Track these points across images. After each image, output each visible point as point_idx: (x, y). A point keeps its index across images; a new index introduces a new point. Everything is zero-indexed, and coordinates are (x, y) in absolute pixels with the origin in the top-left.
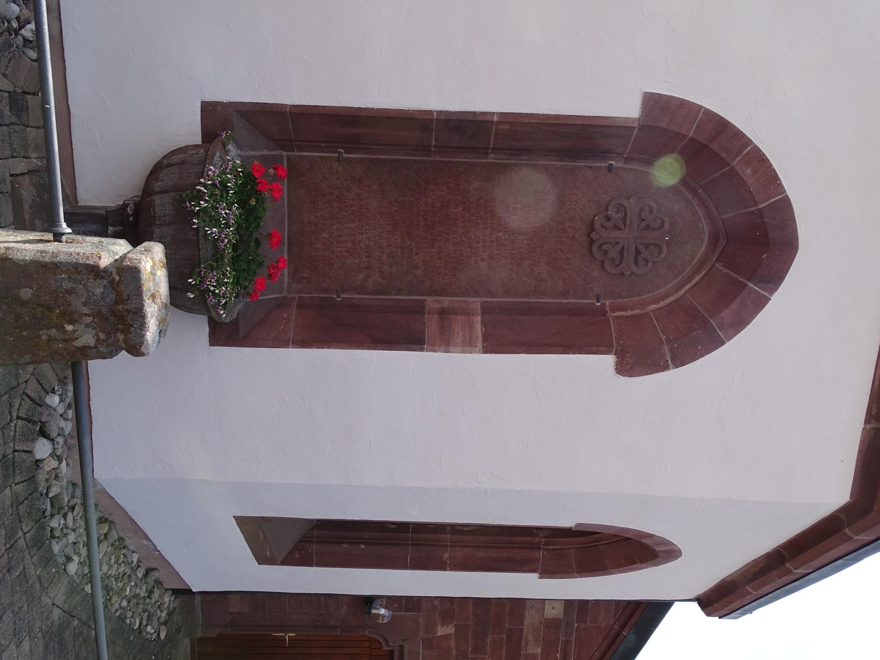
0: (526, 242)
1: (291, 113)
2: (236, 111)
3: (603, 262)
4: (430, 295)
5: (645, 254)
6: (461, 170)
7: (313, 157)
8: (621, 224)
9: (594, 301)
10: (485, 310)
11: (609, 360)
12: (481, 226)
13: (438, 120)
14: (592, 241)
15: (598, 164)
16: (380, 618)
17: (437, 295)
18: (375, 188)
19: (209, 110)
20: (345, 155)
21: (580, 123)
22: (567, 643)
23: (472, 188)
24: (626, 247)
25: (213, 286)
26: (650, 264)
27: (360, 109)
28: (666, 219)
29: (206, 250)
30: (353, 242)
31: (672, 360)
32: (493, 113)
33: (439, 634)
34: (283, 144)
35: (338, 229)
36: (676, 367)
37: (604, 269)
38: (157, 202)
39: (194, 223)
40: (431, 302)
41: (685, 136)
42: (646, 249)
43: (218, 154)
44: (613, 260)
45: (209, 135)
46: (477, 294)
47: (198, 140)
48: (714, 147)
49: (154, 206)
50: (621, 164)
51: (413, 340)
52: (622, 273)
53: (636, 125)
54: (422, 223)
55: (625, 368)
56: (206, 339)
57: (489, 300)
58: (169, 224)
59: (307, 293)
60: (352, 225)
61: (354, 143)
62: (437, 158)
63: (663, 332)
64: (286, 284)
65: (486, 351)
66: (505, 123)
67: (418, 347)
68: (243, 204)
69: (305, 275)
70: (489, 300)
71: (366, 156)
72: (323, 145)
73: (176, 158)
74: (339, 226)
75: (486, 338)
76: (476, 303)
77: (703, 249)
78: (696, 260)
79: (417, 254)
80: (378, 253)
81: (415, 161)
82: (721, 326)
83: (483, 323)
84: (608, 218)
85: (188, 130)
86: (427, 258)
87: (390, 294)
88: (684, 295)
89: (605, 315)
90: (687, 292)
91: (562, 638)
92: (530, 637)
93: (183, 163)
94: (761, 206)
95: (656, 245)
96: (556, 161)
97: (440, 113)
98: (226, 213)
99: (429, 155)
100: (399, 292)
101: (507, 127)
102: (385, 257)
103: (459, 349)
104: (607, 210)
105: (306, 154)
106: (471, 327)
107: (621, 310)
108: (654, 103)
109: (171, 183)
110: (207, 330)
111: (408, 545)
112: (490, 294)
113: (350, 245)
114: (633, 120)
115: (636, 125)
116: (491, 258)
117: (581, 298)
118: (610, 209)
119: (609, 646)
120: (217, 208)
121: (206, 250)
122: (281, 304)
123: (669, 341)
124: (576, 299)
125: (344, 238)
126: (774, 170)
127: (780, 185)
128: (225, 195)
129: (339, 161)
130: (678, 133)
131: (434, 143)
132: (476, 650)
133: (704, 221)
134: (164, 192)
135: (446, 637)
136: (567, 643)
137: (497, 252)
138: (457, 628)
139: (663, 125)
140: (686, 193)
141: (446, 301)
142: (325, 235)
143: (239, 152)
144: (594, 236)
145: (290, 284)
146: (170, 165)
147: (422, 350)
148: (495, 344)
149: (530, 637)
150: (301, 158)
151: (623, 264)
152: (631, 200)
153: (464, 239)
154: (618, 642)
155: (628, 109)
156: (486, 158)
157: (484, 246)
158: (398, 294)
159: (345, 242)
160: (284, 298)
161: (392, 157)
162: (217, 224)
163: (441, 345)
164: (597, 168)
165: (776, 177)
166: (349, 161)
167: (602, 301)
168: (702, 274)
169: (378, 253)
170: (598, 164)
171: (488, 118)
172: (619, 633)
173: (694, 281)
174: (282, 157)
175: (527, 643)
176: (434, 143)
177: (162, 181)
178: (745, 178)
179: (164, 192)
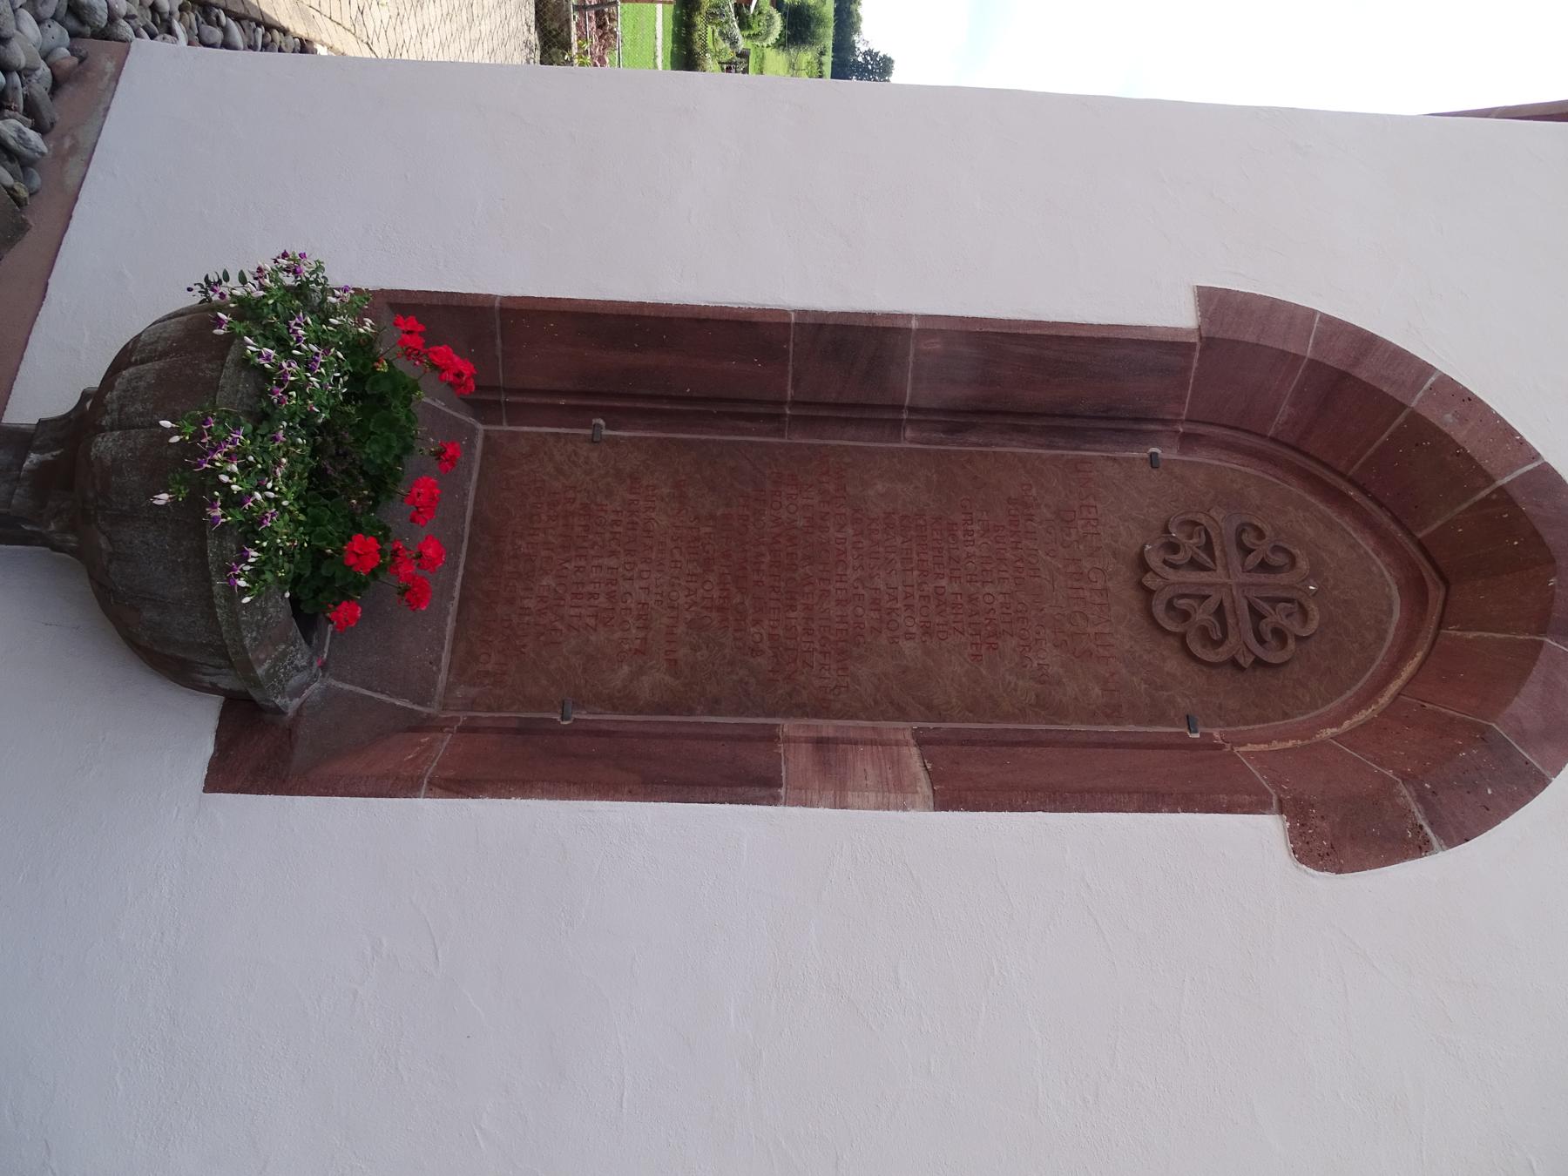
0: (1001, 598)
2: (391, 305)
4: (788, 714)
7: (540, 434)
8: (1203, 557)
9: (1185, 730)
12: (899, 565)
14: (1149, 593)
15: (1127, 454)
17: (806, 715)
18: (666, 491)
20: (605, 432)
21: (1083, 334)
23: (871, 492)
24: (1227, 604)
25: (231, 475)
26: (1291, 644)
30: (611, 596)
31: (1431, 824)
32: (909, 316)
35: (578, 568)
41: (1297, 358)
44: (1204, 631)
48: (1362, 374)
50: (1173, 455)
51: (747, 779)
53: (1194, 339)
54: (767, 559)
56: (199, 771)
57: (931, 725)
59: (489, 709)
60: (613, 562)
64: (441, 686)
67: (764, 792)
69: (489, 667)
70: (931, 725)
74: (583, 563)
77: (1396, 616)
78: (1390, 637)
79: (757, 622)
80: (665, 620)
81: (751, 443)
84: (1173, 547)
86: (781, 632)
87: (691, 712)
94: (1501, 482)
96: (1041, 446)
99: (779, 432)
100: (714, 707)
102: (681, 629)
105: (526, 429)
110: (209, 749)
111: (795, 404)
113: (602, 601)
114: (1188, 332)
116: (927, 631)
117: (1151, 722)
123: (1407, 778)
124: (1138, 723)
125: (590, 588)
126: (1497, 416)
131: (790, 392)
133: (1379, 562)
137: (938, 620)
140: (1322, 507)
141: (827, 727)
142: (547, 581)
144: (1149, 581)
145: (449, 688)
147: (774, 800)
150: (514, 436)
151: (1232, 639)
153: (861, 591)
155: (1177, 314)
157: (908, 607)
158: (711, 713)
159: (592, 595)
161: (704, 437)
164: (1127, 460)
166: (615, 442)
168: (1416, 660)
169: (665, 620)
170: (1127, 454)
171: (900, 324)
174: (474, 430)
176: (790, 392)
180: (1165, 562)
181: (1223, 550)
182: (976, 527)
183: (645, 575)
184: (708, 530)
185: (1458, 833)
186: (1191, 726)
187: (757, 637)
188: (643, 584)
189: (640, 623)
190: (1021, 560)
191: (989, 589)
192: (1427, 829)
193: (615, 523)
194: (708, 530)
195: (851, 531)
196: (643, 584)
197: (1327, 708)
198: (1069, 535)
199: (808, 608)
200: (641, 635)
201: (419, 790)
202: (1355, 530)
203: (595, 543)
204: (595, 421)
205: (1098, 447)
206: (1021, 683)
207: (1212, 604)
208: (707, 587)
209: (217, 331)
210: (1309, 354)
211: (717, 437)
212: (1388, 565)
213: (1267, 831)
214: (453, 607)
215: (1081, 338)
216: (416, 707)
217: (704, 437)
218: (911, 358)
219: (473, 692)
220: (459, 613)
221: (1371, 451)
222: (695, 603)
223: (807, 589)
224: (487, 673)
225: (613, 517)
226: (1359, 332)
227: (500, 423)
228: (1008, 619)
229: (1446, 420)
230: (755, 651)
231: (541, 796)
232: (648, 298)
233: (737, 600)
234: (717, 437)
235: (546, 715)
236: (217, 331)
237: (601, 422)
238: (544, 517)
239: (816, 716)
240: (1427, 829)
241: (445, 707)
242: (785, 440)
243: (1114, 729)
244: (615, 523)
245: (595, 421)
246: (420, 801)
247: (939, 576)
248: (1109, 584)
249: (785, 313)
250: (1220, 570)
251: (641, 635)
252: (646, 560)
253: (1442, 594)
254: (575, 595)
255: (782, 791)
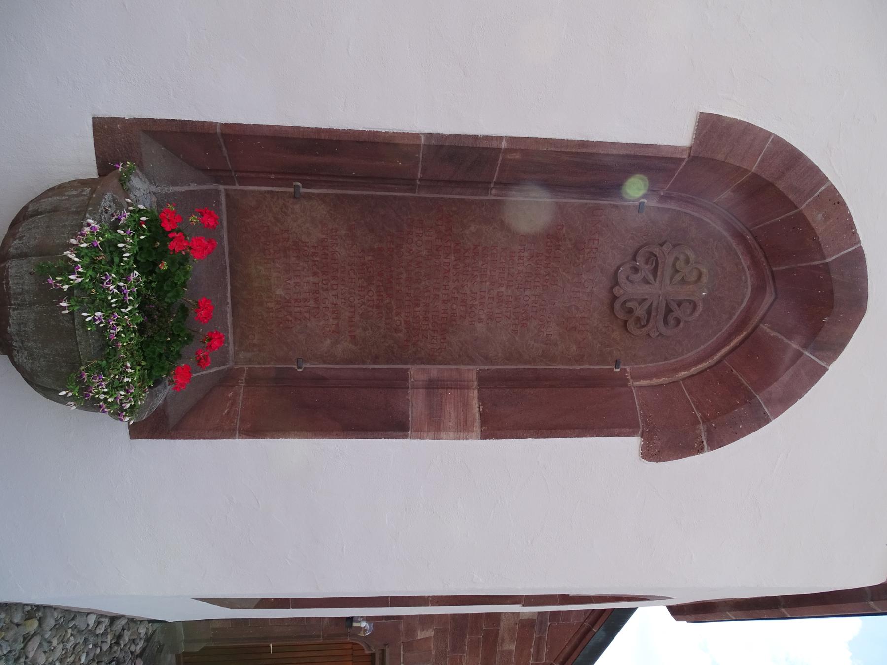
0: (533, 298)
1: (222, 134)
3: (626, 322)
5: (677, 313)
6: (454, 209)
7: (260, 192)
9: (613, 367)
10: (484, 381)
11: (633, 443)
12: (479, 279)
13: (428, 147)
14: (615, 298)
16: (362, 632)
17: (423, 363)
18: (343, 232)
19: (104, 128)
20: (302, 190)
21: (615, 152)
22: (540, 639)
23: (467, 232)
24: (655, 305)
25: (105, 393)
27: (319, 130)
28: (704, 270)
29: (86, 346)
30: (316, 300)
31: (708, 441)
32: (501, 138)
33: (419, 638)
34: (219, 175)
35: (296, 284)
36: (712, 449)
37: (626, 329)
38: (12, 272)
39: (64, 308)
40: (417, 373)
41: (746, 171)
42: (679, 306)
43: (108, 196)
44: (638, 319)
45: (105, 166)
46: (472, 361)
47: (91, 171)
48: (781, 185)
49: (7, 278)
51: (393, 425)
52: (649, 335)
54: (404, 276)
55: (650, 453)
57: (486, 367)
58: (31, 304)
59: (259, 363)
61: (311, 174)
62: (423, 194)
63: (697, 408)
65: (485, 436)
66: (515, 151)
67: (401, 434)
68: (148, 268)
69: (255, 341)
70: (486, 367)
71: (330, 191)
72: (273, 176)
73: (46, 204)
74: (298, 280)
75: (484, 420)
76: (470, 372)
78: (735, 317)
79: (398, 314)
81: (395, 197)
82: (768, 402)
83: (481, 399)
84: (636, 270)
85: (78, 159)
87: (364, 363)
88: (720, 361)
89: (626, 386)
90: (724, 356)
91: (535, 635)
92: (506, 636)
93: (55, 210)
94: (829, 260)
95: (690, 302)
97: (430, 136)
98: (119, 288)
99: (413, 190)
101: (518, 156)
102: (357, 318)
103: (452, 434)
104: (634, 258)
106: (466, 405)
107: (645, 377)
108: (711, 127)
109: (33, 242)
112: (488, 360)
113: (312, 303)
114: (683, 149)
115: (685, 156)
116: (490, 318)
117: (598, 364)
118: (638, 259)
119: (580, 641)
120: (102, 282)
121: (86, 346)
122: (227, 379)
123: (706, 420)
124: (590, 364)
125: (304, 295)
126: (850, 216)
127: (855, 234)
128: (117, 259)
129: (294, 197)
130: (739, 168)
131: (420, 175)
132: (454, 649)
133: (747, 273)
134: (22, 255)
135: (426, 640)
136: (540, 639)
138: (437, 631)
139: (720, 157)
141: (435, 370)
143: (153, 188)
144: (616, 290)
145: (236, 353)
146: (37, 213)
147: (405, 437)
148: (494, 428)
149: (506, 636)
151: (651, 325)
152: (664, 248)
153: (456, 295)
154: (588, 637)
156: (487, 194)
157: (481, 304)
158: (375, 363)
159: (306, 300)
160: (230, 370)
161: (365, 193)
162: (105, 305)
163: (428, 431)
165: (851, 225)
166: (309, 197)
167: (621, 367)
168: (745, 333)
169: (347, 314)
171: (495, 145)
172: (589, 630)
173: (732, 344)
174: (218, 192)
175: (503, 640)
176: (420, 175)
177: (21, 239)
178: (813, 225)
179: (22, 255)
180: (627, 278)
181: (662, 272)
182: (526, 254)
183: (335, 287)
184: (370, 258)
185: (716, 443)
186: (617, 365)
187: (398, 323)
188: (334, 292)
189: (334, 316)
190: (549, 275)
191: (527, 292)
192: (705, 443)
193: (314, 254)
194: (370, 258)
195: (453, 258)
196: (334, 292)
197: (689, 354)
198: (579, 259)
199: (426, 305)
200: (336, 322)
201: (235, 435)
202: (742, 254)
203: (304, 268)
204: (294, 183)
205: (609, 199)
206: (536, 345)
207: (646, 305)
208: (370, 293)
209: (63, 312)
210: (754, 170)
211: (374, 193)
212: (752, 276)
213: (630, 445)
214: (229, 309)
215: (612, 155)
216: (221, 368)
217: (365, 193)
218: (499, 162)
219: (249, 355)
220: (233, 312)
221: (768, 223)
222: (364, 304)
223: (426, 294)
224: (254, 345)
225: (313, 250)
226: (794, 149)
227: (234, 185)
228: (535, 310)
229: (817, 219)
230: (397, 330)
231: (295, 437)
232: (323, 126)
233: (388, 301)
234: (374, 193)
235: (289, 366)
236: (63, 312)
237: (299, 184)
238: (272, 251)
239: (429, 363)
240: (705, 443)
241: (236, 363)
242: (416, 195)
243: (578, 367)
244: (314, 254)
245: (294, 183)
246: (237, 441)
247: (501, 285)
248: (594, 289)
249: (416, 136)
250: (657, 284)
251: (336, 322)
252: (334, 278)
253: (770, 301)
254: (296, 300)
255: (409, 433)
